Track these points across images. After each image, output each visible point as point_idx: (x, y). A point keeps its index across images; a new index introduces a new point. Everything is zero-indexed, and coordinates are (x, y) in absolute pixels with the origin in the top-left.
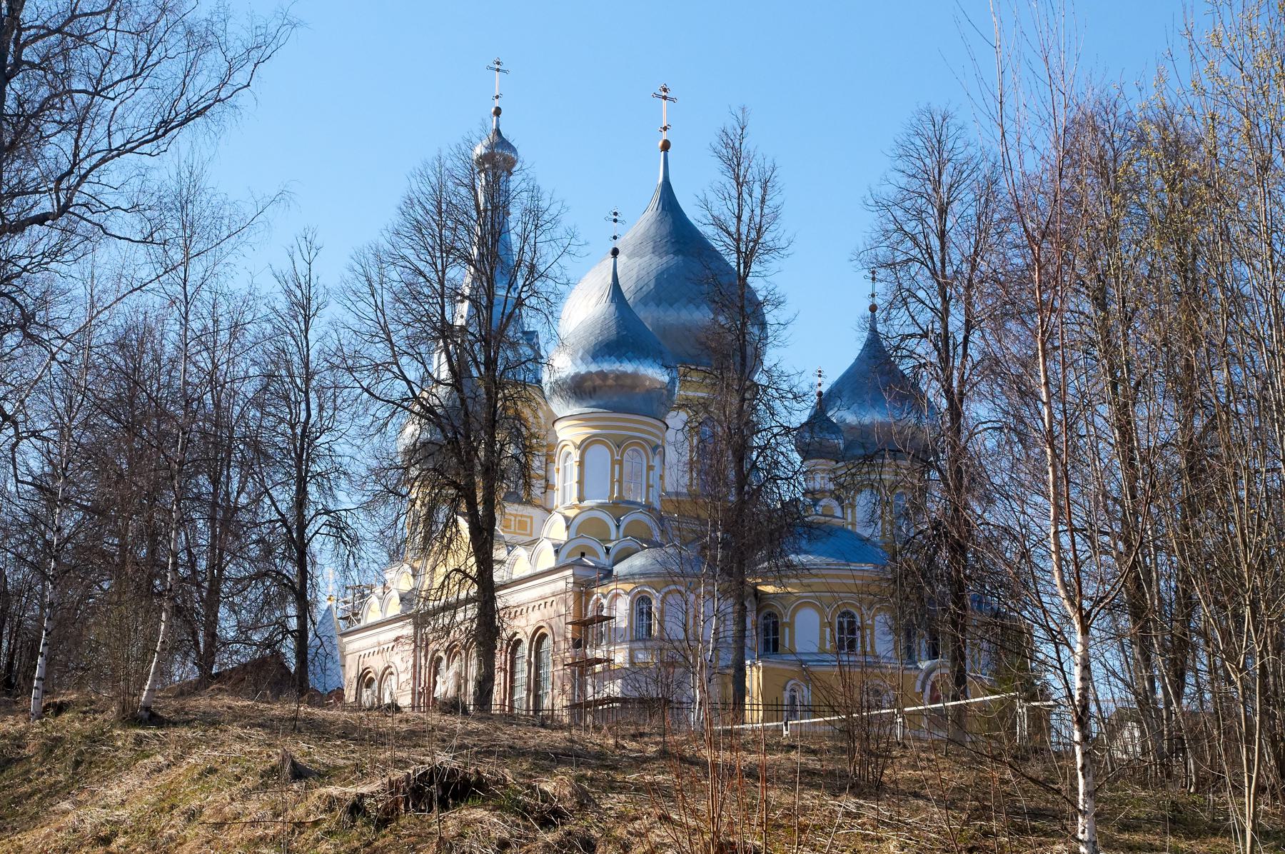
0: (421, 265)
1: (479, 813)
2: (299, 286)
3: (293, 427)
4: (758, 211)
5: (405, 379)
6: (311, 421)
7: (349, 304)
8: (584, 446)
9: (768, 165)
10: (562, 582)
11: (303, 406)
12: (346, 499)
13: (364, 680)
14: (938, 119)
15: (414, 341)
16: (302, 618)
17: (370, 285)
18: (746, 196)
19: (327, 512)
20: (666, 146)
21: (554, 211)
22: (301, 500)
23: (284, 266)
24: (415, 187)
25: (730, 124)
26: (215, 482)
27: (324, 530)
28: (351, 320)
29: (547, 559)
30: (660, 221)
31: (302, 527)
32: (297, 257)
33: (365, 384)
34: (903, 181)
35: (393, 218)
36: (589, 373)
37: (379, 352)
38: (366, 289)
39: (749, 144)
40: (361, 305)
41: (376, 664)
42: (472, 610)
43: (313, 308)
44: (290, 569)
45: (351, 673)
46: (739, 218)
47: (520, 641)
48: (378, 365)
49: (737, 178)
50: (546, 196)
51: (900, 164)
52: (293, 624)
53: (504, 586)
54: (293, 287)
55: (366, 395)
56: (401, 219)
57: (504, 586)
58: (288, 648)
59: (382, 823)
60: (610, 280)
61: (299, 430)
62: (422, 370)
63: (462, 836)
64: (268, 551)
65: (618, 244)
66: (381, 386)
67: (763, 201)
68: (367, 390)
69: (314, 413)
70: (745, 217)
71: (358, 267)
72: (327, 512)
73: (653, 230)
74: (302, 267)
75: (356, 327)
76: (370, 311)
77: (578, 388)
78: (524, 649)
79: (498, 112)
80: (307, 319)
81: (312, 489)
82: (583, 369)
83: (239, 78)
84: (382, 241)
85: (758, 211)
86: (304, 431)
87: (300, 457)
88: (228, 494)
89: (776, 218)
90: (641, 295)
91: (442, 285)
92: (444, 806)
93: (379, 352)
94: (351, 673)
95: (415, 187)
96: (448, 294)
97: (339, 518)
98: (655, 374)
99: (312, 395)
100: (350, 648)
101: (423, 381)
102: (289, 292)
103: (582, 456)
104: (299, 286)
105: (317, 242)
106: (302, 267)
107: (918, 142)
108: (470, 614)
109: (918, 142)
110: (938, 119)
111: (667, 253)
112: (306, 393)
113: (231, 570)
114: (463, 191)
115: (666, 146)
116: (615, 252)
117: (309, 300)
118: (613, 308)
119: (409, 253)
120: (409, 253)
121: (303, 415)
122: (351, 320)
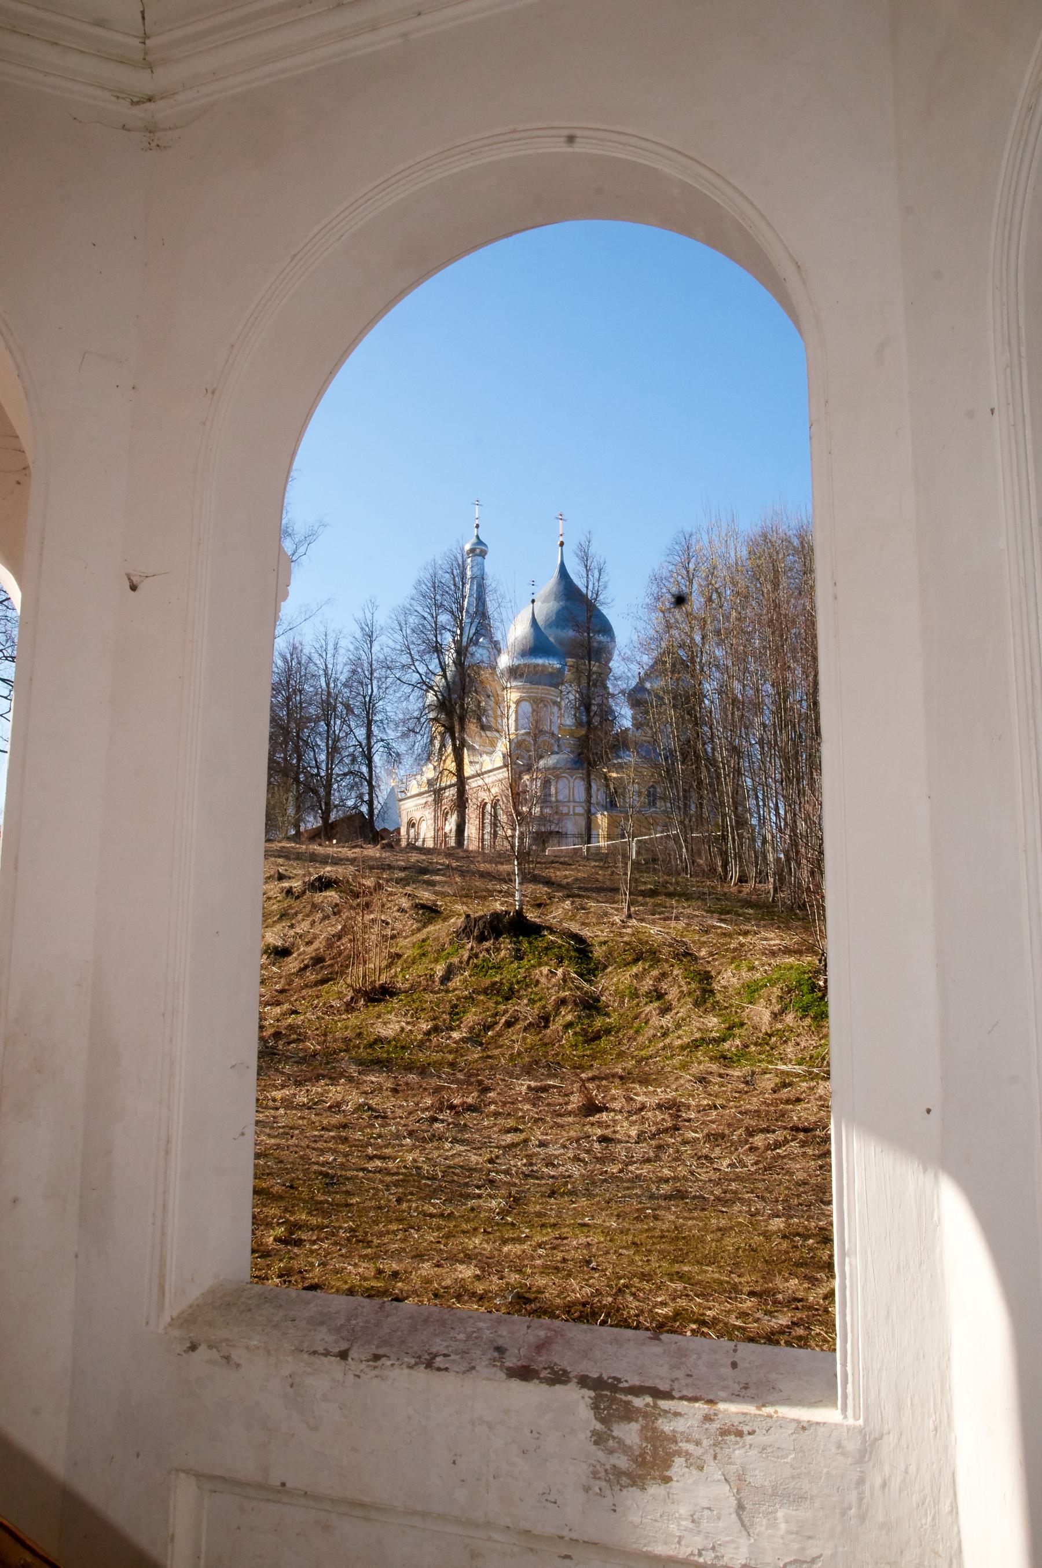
0: (426, 615)
1: (333, 893)
2: (367, 626)
3: (364, 697)
4: (596, 584)
5: (418, 672)
6: (374, 693)
7: (389, 635)
8: (518, 703)
9: (602, 561)
10: (504, 774)
11: (370, 686)
12: (391, 734)
13: (411, 824)
14: (687, 536)
15: (422, 654)
16: (370, 794)
17: (400, 625)
18: (590, 576)
19: (382, 740)
20: (562, 544)
21: (493, 585)
22: (369, 734)
23: (360, 615)
24: (422, 575)
25: (583, 540)
26: (328, 725)
27: (382, 749)
28: (391, 643)
29: (499, 763)
30: (559, 583)
31: (370, 748)
32: (367, 611)
33: (397, 676)
34: (671, 567)
35: (411, 591)
36: (519, 665)
37: (405, 659)
38: (398, 628)
39: (592, 550)
40: (395, 635)
41: (417, 816)
42: (453, 791)
43: (374, 637)
44: (364, 769)
45: (405, 820)
46: (587, 587)
47: (486, 803)
48: (404, 666)
49: (586, 566)
50: (490, 578)
51: (670, 558)
52: (366, 798)
53: (469, 778)
54: (364, 626)
55: (398, 681)
56: (414, 591)
57: (469, 778)
58: (364, 809)
59: (298, 897)
60: (531, 616)
61: (367, 699)
62: (426, 668)
63: (322, 902)
64: (354, 760)
65: (534, 597)
66: (407, 676)
67: (599, 580)
68: (399, 679)
69: (375, 690)
70: (590, 587)
71: (393, 616)
72: (382, 740)
73: (555, 589)
74: (369, 616)
75: (393, 647)
76: (400, 638)
77: (514, 672)
78: (489, 807)
79: (477, 526)
80: (371, 642)
81: (374, 728)
82: (516, 662)
83: (301, 550)
84: (406, 602)
85: (596, 584)
86: (370, 699)
87: (368, 713)
88: (334, 731)
89: (605, 587)
90: (548, 622)
91: (436, 625)
92: (321, 891)
93: (405, 659)
94: (405, 820)
95: (422, 575)
96: (437, 629)
97: (388, 744)
98: (554, 663)
99: (375, 682)
100: (402, 807)
101: (426, 673)
102: (362, 629)
103: (517, 707)
104: (367, 626)
105: (376, 603)
106: (369, 616)
107: (677, 548)
108: (452, 792)
109: (677, 548)
110: (687, 536)
111: (562, 600)
112: (371, 680)
113: (336, 770)
114: (447, 576)
115: (562, 544)
116: (533, 601)
117: (372, 632)
118: (532, 630)
119: (419, 609)
120: (419, 609)
121: (370, 692)
122: (391, 643)
